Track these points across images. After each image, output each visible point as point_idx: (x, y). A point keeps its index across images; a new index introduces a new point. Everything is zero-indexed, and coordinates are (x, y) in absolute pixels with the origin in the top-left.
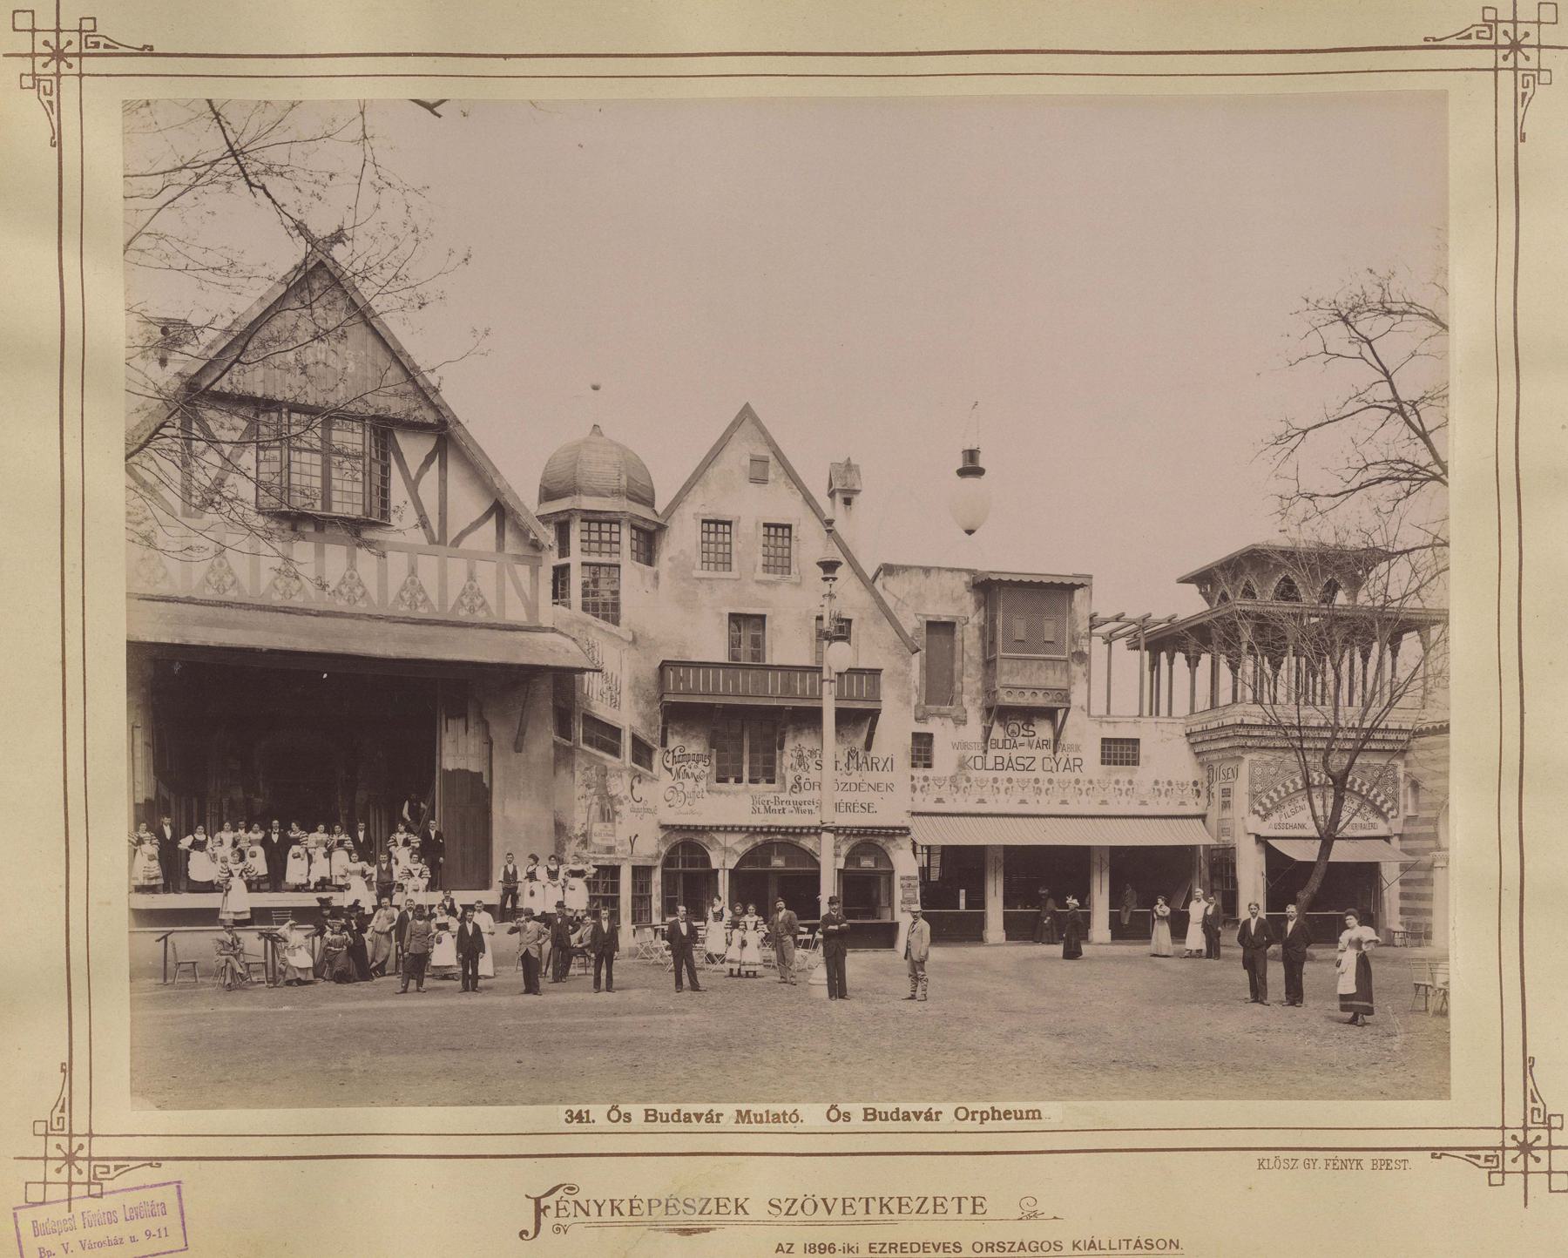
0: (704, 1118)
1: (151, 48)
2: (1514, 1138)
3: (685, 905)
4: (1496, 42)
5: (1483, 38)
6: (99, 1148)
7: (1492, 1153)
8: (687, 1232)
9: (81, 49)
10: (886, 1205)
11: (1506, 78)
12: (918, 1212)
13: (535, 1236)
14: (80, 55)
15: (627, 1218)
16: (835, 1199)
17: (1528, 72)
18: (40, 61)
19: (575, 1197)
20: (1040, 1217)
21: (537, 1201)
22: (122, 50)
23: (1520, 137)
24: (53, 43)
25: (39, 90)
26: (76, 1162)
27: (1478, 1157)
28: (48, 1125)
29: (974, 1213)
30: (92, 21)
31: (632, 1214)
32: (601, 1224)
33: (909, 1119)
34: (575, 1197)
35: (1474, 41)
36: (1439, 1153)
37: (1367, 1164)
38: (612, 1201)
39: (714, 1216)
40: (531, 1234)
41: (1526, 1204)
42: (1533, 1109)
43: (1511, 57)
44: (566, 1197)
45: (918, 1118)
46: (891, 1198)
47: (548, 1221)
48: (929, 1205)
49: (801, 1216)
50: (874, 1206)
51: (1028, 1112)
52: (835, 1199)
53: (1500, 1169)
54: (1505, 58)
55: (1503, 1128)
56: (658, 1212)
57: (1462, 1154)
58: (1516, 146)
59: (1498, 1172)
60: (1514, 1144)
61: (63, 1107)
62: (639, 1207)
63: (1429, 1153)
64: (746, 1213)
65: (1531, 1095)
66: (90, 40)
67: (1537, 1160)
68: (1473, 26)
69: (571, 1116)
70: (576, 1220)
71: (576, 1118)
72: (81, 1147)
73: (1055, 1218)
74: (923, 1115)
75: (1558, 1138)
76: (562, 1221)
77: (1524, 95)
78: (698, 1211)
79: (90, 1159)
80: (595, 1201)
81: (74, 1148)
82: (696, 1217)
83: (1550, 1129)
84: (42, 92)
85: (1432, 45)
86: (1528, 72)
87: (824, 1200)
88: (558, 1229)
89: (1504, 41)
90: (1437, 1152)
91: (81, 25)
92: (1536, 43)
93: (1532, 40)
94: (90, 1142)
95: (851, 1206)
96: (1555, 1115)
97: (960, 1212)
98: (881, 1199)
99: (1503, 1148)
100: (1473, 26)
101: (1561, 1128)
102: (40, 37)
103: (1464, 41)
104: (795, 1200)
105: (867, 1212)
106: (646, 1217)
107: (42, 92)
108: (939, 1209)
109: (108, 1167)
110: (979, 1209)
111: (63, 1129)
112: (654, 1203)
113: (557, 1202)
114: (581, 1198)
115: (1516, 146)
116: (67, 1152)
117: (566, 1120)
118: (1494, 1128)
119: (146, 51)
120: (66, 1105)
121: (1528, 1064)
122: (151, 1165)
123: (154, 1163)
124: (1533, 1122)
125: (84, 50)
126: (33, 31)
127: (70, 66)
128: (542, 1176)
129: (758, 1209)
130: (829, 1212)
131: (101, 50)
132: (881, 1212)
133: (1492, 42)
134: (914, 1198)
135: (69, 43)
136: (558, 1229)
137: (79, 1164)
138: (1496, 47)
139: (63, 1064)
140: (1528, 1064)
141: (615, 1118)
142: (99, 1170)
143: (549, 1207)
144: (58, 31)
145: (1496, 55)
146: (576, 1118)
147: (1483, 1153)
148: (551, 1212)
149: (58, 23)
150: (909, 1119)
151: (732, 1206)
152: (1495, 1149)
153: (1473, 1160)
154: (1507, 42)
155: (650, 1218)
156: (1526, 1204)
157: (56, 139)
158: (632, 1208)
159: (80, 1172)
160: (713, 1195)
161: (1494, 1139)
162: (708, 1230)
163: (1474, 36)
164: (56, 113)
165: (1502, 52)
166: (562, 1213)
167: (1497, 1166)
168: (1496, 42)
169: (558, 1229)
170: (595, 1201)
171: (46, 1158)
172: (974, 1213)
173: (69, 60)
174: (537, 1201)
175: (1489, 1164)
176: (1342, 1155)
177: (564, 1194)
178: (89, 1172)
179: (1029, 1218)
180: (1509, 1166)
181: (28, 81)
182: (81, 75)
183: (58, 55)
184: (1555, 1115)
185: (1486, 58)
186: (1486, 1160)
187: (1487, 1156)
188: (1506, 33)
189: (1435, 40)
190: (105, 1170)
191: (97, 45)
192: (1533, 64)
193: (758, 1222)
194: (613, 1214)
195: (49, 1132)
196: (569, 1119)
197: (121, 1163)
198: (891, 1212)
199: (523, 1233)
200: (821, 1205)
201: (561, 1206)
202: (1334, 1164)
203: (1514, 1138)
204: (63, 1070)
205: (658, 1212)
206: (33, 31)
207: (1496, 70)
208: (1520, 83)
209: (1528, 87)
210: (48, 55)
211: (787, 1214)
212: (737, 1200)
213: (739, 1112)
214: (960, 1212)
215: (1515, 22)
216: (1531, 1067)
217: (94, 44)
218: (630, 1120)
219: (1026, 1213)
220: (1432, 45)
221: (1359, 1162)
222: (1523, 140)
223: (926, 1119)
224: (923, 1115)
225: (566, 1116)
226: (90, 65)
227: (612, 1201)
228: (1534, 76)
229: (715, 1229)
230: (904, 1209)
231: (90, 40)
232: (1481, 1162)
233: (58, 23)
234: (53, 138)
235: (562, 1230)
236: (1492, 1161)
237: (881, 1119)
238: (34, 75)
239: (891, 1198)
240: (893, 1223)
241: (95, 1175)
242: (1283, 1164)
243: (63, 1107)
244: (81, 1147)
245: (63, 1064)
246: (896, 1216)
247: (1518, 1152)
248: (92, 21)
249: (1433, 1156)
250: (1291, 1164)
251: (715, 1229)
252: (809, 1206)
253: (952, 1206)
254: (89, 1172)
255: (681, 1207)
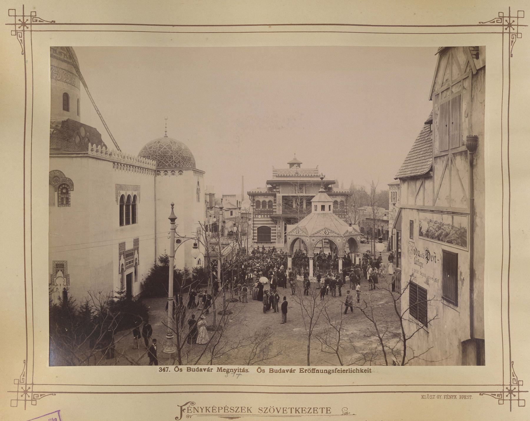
0: (206, 370)
1: (55, 22)
2: (507, 388)
3: (193, 292)
4: (503, 24)
5: (499, 22)
6: (36, 388)
7: (500, 393)
8: (232, 418)
9: (31, 22)
10: (297, 410)
11: (506, 36)
12: (308, 413)
13: (181, 418)
14: (31, 24)
15: (211, 413)
16: (281, 408)
17: (514, 34)
18: (17, 26)
19: (194, 406)
20: (348, 414)
21: (181, 407)
22: (45, 22)
23: (511, 55)
24: (22, 20)
25: (17, 36)
26: (28, 393)
27: (495, 395)
28: (19, 381)
29: (327, 413)
30: (35, 13)
31: (213, 412)
32: (201, 416)
33: (285, 372)
34: (194, 406)
35: (496, 23)
36: (482, 393)
37: (458, 397)
38: (206, 407)
39: (240, 413)
40: (179, 418)
41: (511, 410)
42: (513, 379)
43: (508, 29)
44: (191, 406)
45: (287, 372)
46: (299, 408)
47: (185, 414)
48: (312, 410)
49: (269, 413)
50: (294, 411)
51: (325, 370)
52: (281, 408)
53: (502, 399)
54: (506, 29)
55: (503, 385)
56: (222, 412)
57: (490, 394)
58: (509, 58)
59: (33, 16)
60: (507, 390)
61: (24, 374)
62: (215, 410)
63: (479, 393)
64: (251, 412)
65: (512, 374)
66: (34, 19)
67: (515, 396)
68: (495, 18)
69: (161, 369)
70: (194, 413)
71: (163, 370)
72: (29, 388)
73: (354, 414)
74: (289, 371)
75: (521, 388)
76: (190, 414)
77: (512, 41)
78: (235, 411)
79: (32, 392)
80: (201, 407)
81: (27, 389)
82: (234, 413)
83: (519, 385)
84: (18, 37)
85: (481, 25)
86: (514, 34)
87: (277, 408)
88: (188, 416)
89: (506, 23)
90: (481, 393)
91: (31, 14)
92: (517, 24)
93: (515, 23)
94: (32, 386)
95: (286, 410)
96: (520, 381)
97: (322, 413)
98: (296, 408)
99: (503, 392)
100: (495, 18)
101: (522, 385)
102: (17, 18)
103: (492, 23)
104: (267, 408)
105: (291, 413)
106: (217, 413)
107: (18, 37)
108: (315, 412)
109: (38, 395)
110: (328, 412)
111: (512, 35)
112: (220, 408)
113: (188, 408)
114: (195, 406)
115: (509, 58)
116: (25, 390)
117: (159, 371)
118: (500, 385)
119: (53, 23)
120: (25, 374)
121: (511, 363)
122: (53, 395)
123: (54, 394)
124: (513, 383)
125: (32, 23)
126: (15, 16)
127: (28, 28)
128: (183, 399)
129: (255, 411)
130: (278, 412)
131: (38, 22)
132: (296, 413)
133: (502, 24)
134: (307, 408)
135: (27, 20)
136: (188, 416)
137: (29, 394)
138: (503, 25)
139: (24, 360)
140: (511, 363)
141: (177, 370)
142: (35, 396)
143: (185, 409)
144: (23, 16)
145: (503, 28)
146: (163, 370)
147: (497, 394)
148: (186, 411)
149: (23, 13)
150: (285, 372)
151: (246, 410)
152: (501, 392)
153: (41, 20)
154: (507, 24)
155: (219, 413)
156: (511, 410)
157: (23, 52)
158: (213, 410)
159: (29, 396)
160: (240, 406)
161: (500, 389)
162: (238, 418)
163: (496, 22)
164: (44, 394)
165: (505, 27)
166: (189, 411)
167: (501, 398)
168: (503, 24)
169: (188, 416)
170: (201, 407)
171: (18, 392)
172: (327, 413)
173: (27, 26)
174: (181, 407)
175: (499, 397)
176: (450, 394)
177: (190, 405)
178: (32, 396)
179: (345, 414)
180: (505, 398)
181: (521, 383)
182: (31, 31)
183: (24, 24)
184: (520, 381)
185: (500, 29)
186: (498, 396)
187: (498, 394)
188: (506, 21)
189: (482, 23)
190: (37, 396)
191: (36, 21)
192: (515, 31)
193: (254, 415)
194: (206, 412)
195: (19, 383)
196: (160, 371)
197: (42, 394)
198: (299, 413)
199: (176, 418)
200: (276, 409)
201: (189, 409)
202: (447, 397)
203: (507, 388)
204: (24, 363)
205: (222, 412)
206: (15, 16)
207: (503, 33)
208: (25, 379)
209: (513, 39)
210: (20, 24)
211: (264, 413)
212: (248, 408)
213: (218, 368)
214: (322, 413)
215: (25, 400)
216: (512, 365)
217: (36, 20)
218: (182, 371)
219: (344, 413)
220: (481, 25)
221: (455, 396)
222: (512, 56)
223: (290, 372)
224: (289, 371)
225: (159, 369)
226: (34, 27)
227: (206, 407)
228: (515, 35)
229: (240, 417)
230: (304, 412)
231: (34, 19)
232: (496, 397)
233: (23, 13)
234: (22, 52)
235: (189, 417)
236: (500, 396)
237: (275, 372)
238: (16, 31)
239: (299, 408)
240: (300, 416)
241: (34, 398)
242: (430, 397)
243: (24, 374)
244: (29, 388)
245: (24, 360)
246: (301, 414)
247: (508, 393)
248: (35, 13)
249: (480, 394)
250: (433, 397)
251: (240, 417)
252: (272, 410)
253: (320, 411)
254: (32, 396)
255: (229, 410)
